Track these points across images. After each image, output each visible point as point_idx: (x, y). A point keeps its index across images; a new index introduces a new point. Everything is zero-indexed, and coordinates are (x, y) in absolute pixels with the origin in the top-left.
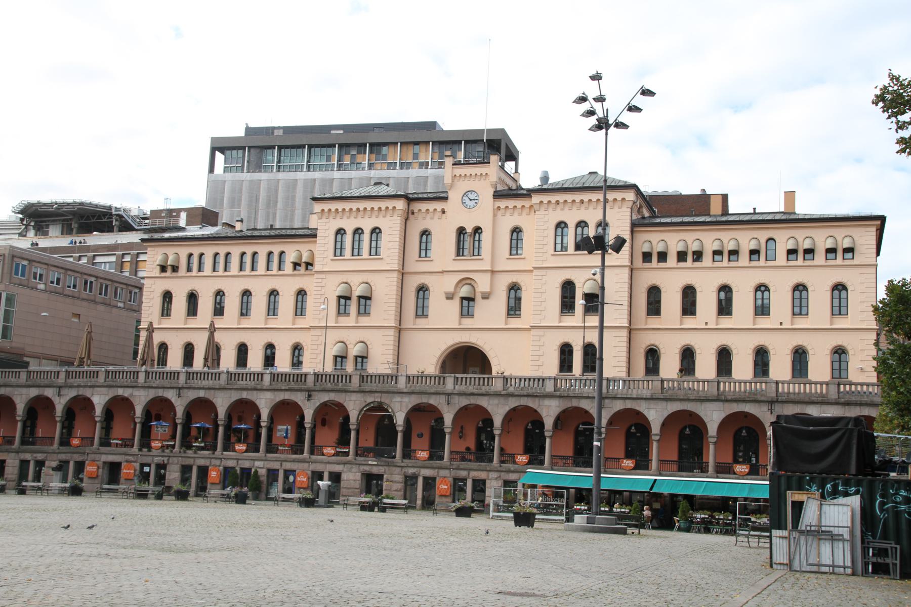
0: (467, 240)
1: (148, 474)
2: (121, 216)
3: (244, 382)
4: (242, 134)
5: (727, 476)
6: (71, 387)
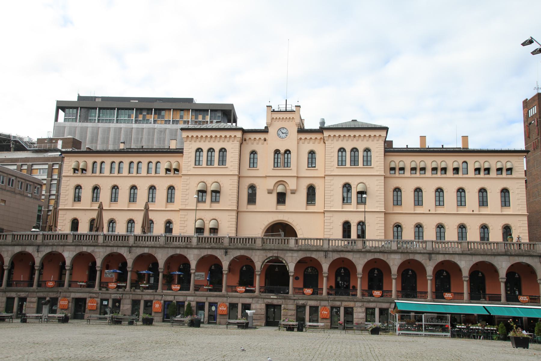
0: (282, 157)
1: (106, 306)
2: (16, 142)
3: (177, 243)
4: (76, 99)
5: (514, 303)
6: (47, 245)
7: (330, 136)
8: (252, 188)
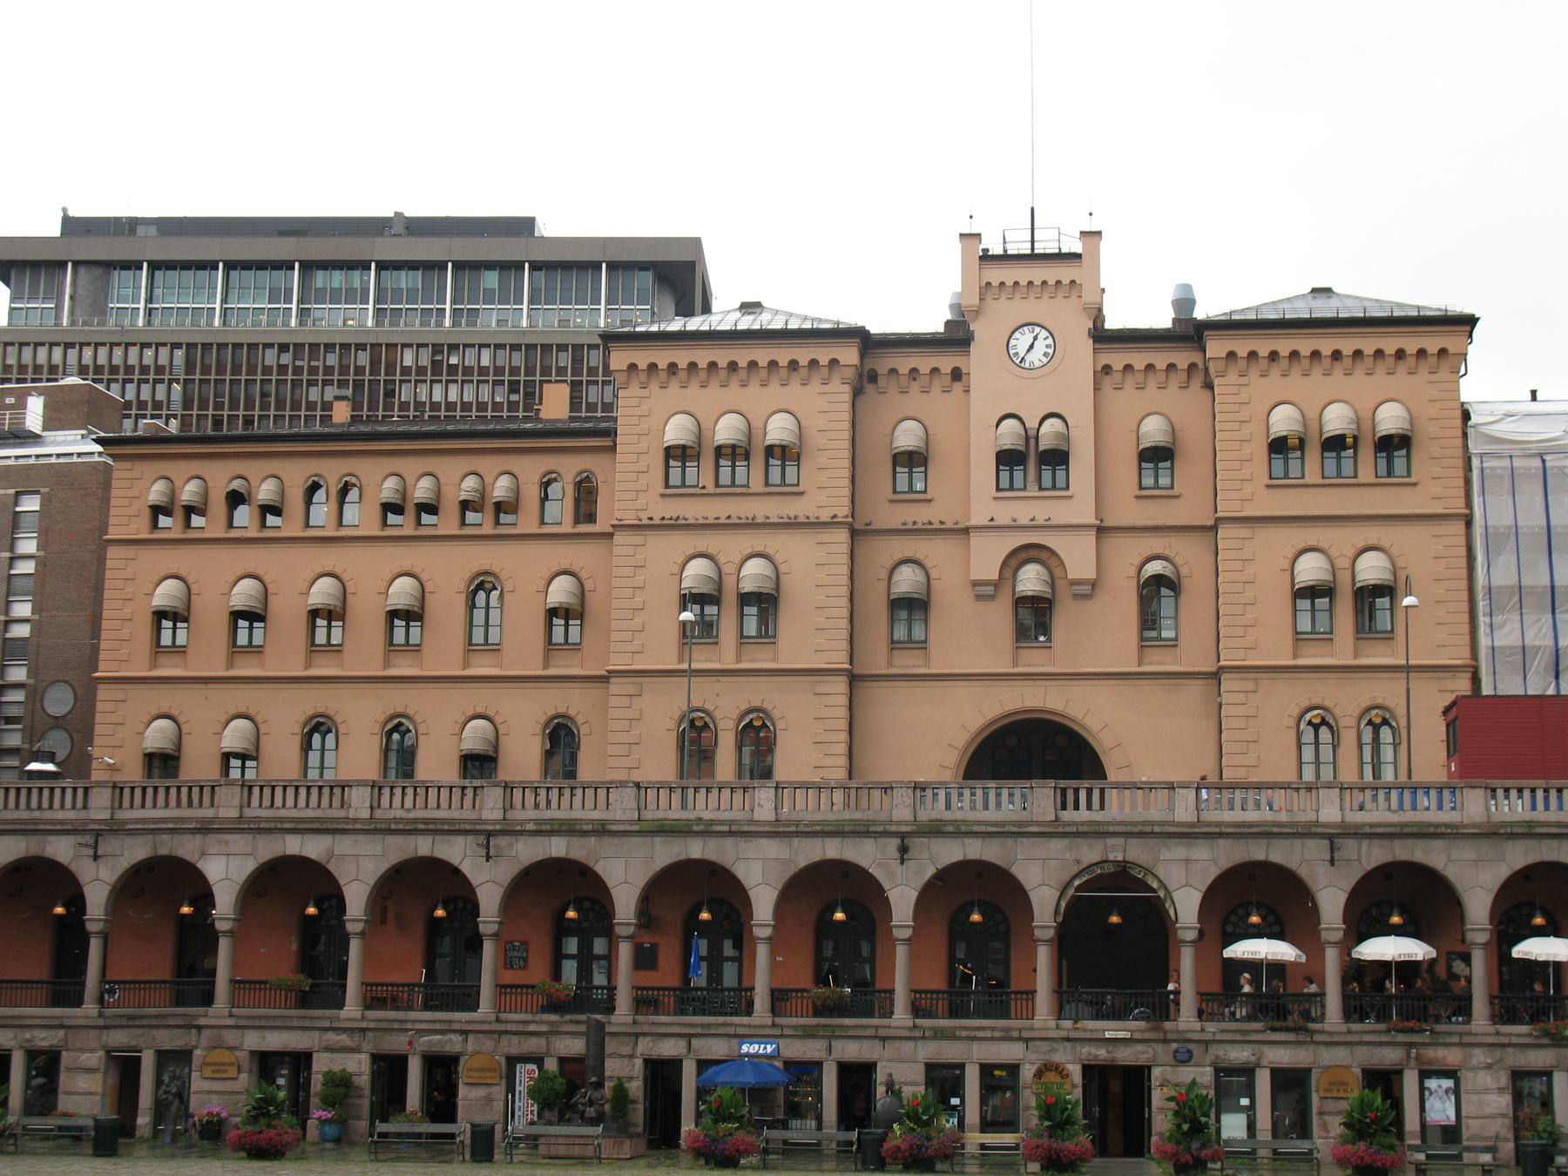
7: (633, 367)
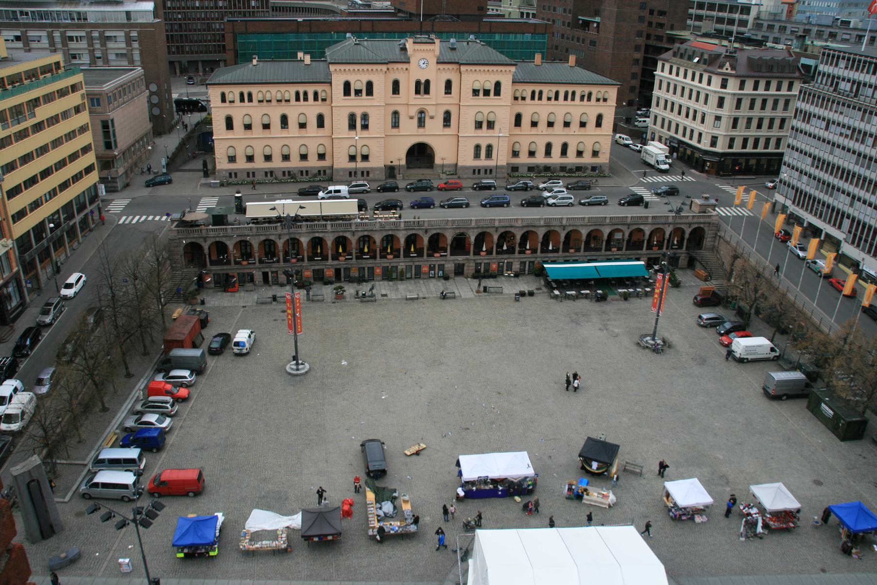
8: (396, 114)
